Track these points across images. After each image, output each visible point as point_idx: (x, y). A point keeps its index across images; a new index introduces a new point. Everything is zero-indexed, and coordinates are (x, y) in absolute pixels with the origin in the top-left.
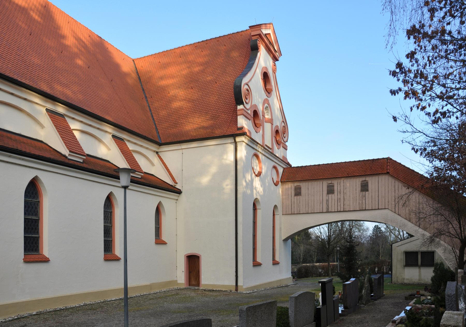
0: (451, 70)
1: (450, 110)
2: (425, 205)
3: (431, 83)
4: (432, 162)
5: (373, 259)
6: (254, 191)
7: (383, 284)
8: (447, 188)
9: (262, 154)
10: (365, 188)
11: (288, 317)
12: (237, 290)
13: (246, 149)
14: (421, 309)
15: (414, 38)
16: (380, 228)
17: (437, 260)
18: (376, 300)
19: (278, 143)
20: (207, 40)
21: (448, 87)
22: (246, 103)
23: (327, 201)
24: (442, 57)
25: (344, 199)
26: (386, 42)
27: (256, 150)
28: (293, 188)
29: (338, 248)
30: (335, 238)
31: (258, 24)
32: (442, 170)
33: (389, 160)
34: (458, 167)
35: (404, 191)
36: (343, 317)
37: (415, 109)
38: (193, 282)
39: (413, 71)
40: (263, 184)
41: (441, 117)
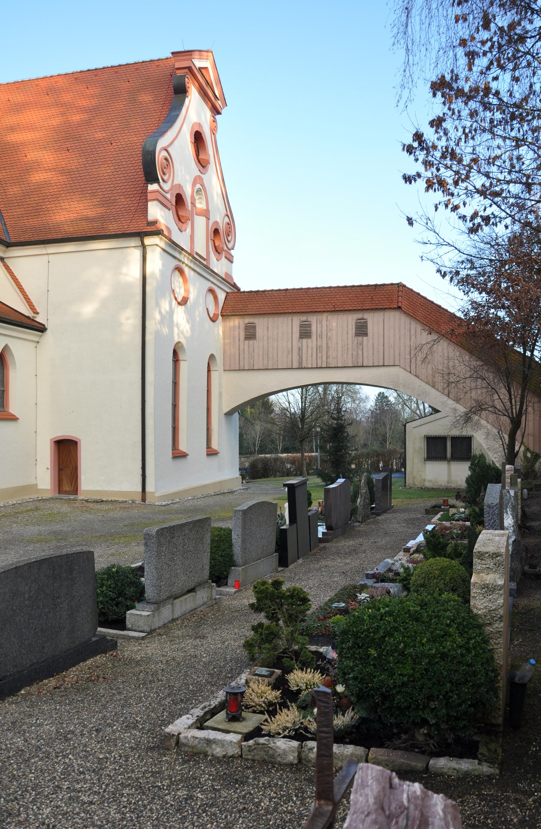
0: (498, 152)
1: (496, 213)
2: (457, 362)
3: (467, 168)
4: (467, 293)
5: (376, 447)
6: (176, 330)
7: (391, 488)
8: (490, 335)
9: (190, 267)
10: (361, 330)
11: (231, 545)
12: (144, 499)
13: (162, 258)
14: (450, 528)
15: (442, 96)
16: (386, 397)
17: (476, 450)
18: (379, 515)
19: (217, 250)
20: (96, 69)
21: (493, 178)
22: (164, 181)
23: (300, 349)
24: (484, 130)
25: (328, 347)
26: (397, 98)
27: (180, 261)
28: (242, 326)
29: (318, 429)
30: (312, 413)
31: (187, 49)
32: (484, 306)
33: (401, 288)
34: (507, 303)
35: (425, 338)
36: (324, 544)
37: (441, 207)
38: (66, 488)
39: (439, 148)
40: (190, 319)
41: (482, 223)
